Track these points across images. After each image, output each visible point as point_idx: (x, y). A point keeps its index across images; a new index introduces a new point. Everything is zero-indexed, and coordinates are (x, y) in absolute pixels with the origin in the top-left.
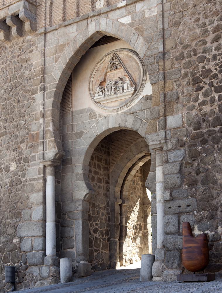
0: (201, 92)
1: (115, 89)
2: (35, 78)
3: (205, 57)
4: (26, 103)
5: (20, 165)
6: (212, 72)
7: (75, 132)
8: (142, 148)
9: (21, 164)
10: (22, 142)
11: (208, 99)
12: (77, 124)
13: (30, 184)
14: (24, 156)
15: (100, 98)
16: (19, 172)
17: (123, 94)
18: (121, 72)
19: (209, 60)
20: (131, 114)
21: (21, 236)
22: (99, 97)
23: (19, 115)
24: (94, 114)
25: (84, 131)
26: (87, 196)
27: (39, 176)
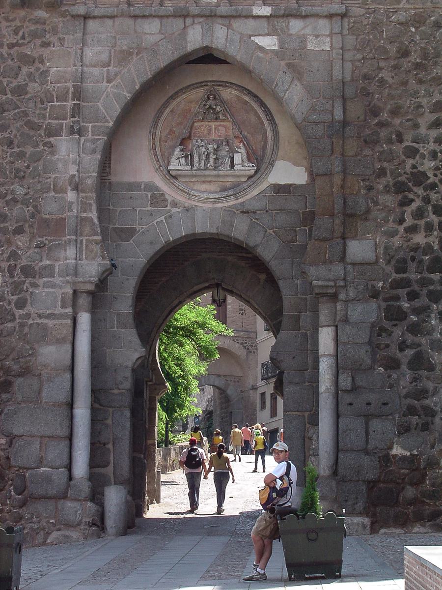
0: (409, 210)
1: (216, 159)
2: (55, 103)
3: (417, 151)
4: (29, 150)
5: (11, 281)
6: (429, 178)
7: (117, 226)
8: (210, 272)
9: (16, 279)
10: (19, 231)
11: (422, 223)
12: (120, 211)
13: (38, 324)
14: (24, 262)
15: (182, 170)
16: (8, 294)
17: (230, 172)
18: (224, 126)
19: (423, 157)
20: (243, 212)
21: (11, 434)
22: (180, 168)
23: (11, 172)
24: (162, 198)
25: (138, 227)
26: (140, 361)
27: (63, 311)
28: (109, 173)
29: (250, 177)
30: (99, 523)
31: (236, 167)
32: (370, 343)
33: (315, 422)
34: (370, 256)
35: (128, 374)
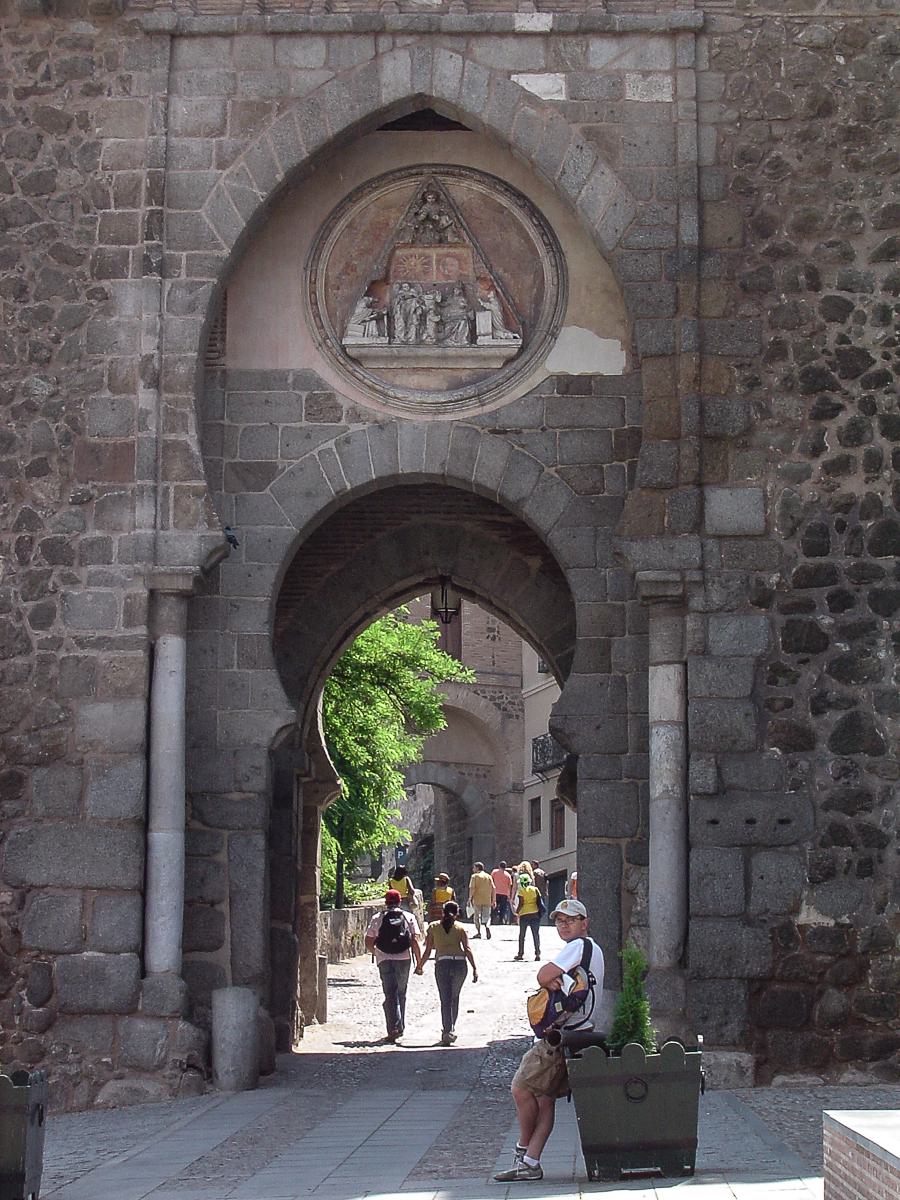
0: (833, 427)
1: (440, 324)
2: (113, 210)
3: (848, 307)
4: (59, 305)
5: (22, 571)
6: (874, 362)
7: (238, 460)
8: (427, 553)
9: (33, 568)
10: (39, 469)
11: (859, 453)
12: (245, 429)
13: (78, 660)
14: (48, 533)
15: (370, 346)
16: (16, 598)
17: (469, 351)
18: (457, 257)
19: (861, 318)
20: (494, 432)
21: (23, 882)
22: (366, 341)
23: (22, 351)
24: (330, 403)
25: (280, 462)
26: (284, 735)
27: (129, 632)
28: (222, 353)
29: (509, 360)
30: (201, 1065)
31: (481, 340)
32: (753, 697)
33: (641, 859)
34: (753, 520)
35: (261, 760)
